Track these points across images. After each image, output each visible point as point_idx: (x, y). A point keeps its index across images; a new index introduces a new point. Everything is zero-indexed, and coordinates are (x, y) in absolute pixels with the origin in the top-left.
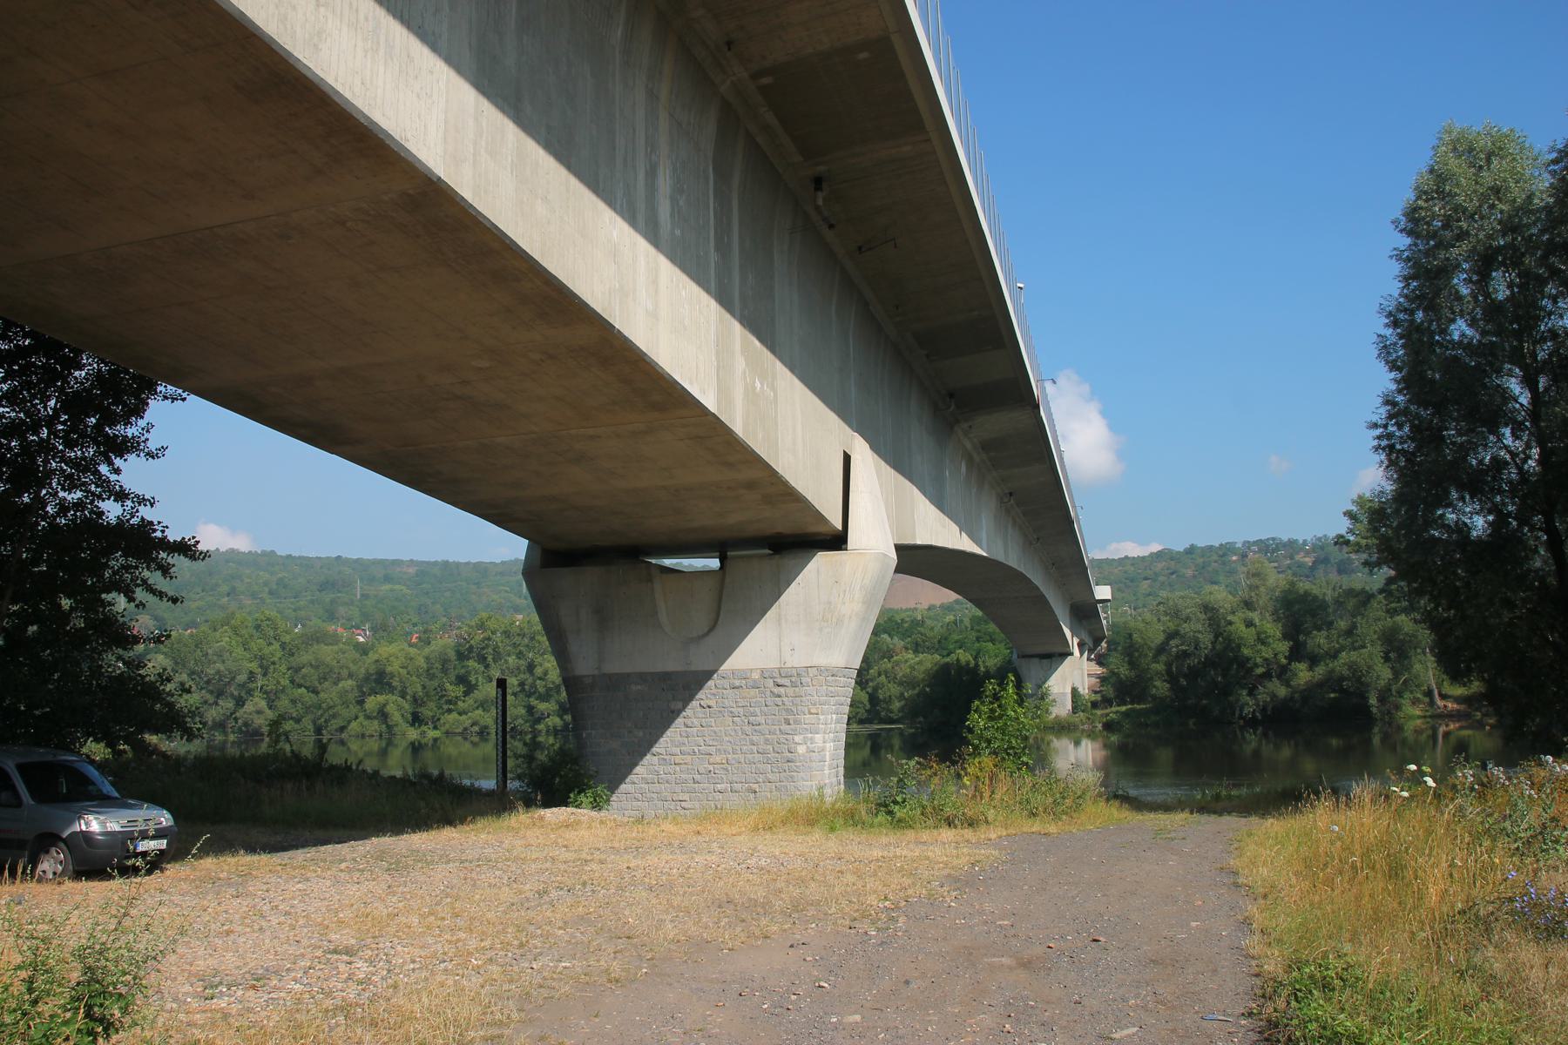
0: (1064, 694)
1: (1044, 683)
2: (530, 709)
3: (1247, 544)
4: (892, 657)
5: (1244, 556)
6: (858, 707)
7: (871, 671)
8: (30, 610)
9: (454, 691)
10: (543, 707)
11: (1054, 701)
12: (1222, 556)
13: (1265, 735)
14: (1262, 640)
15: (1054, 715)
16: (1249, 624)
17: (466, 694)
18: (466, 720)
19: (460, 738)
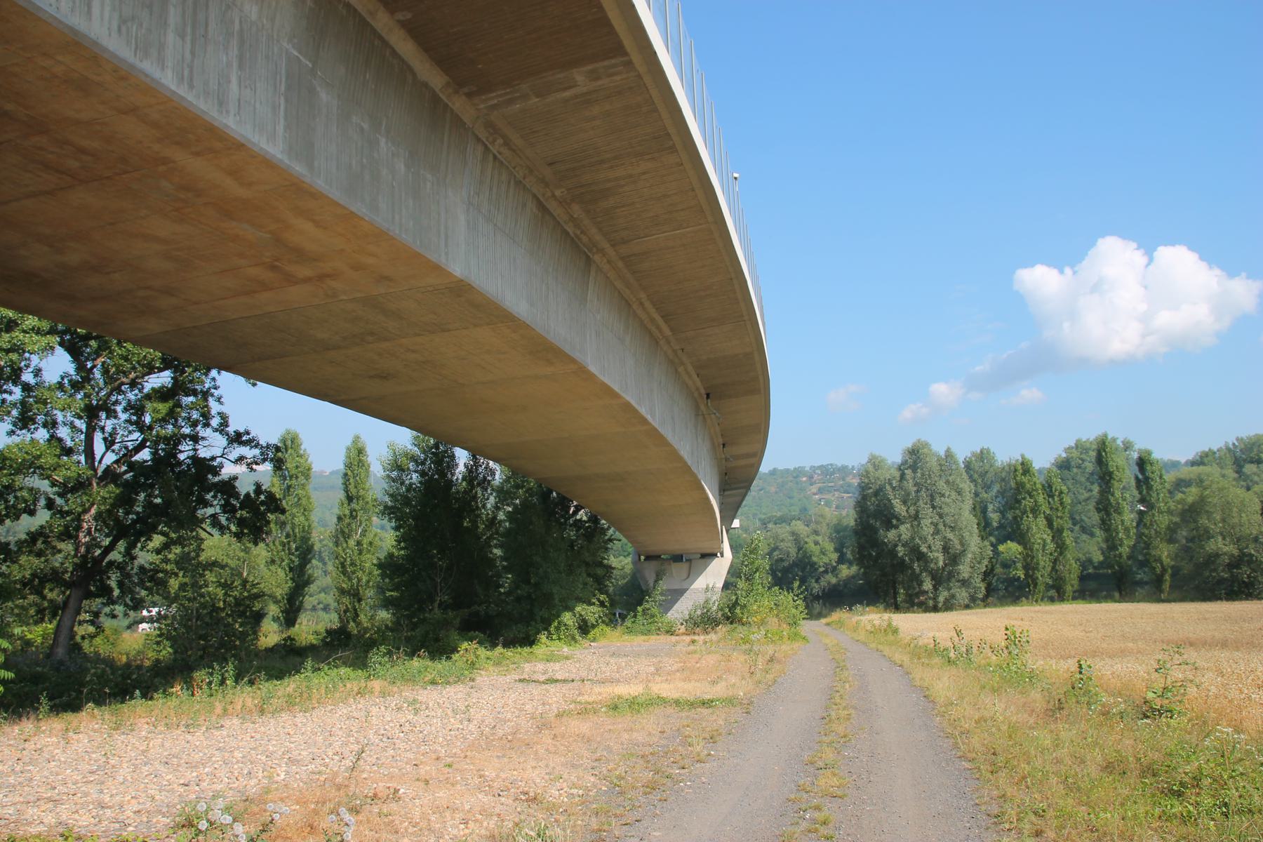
12: (795, 477)
14: (823, 553)
16: (816, 543)
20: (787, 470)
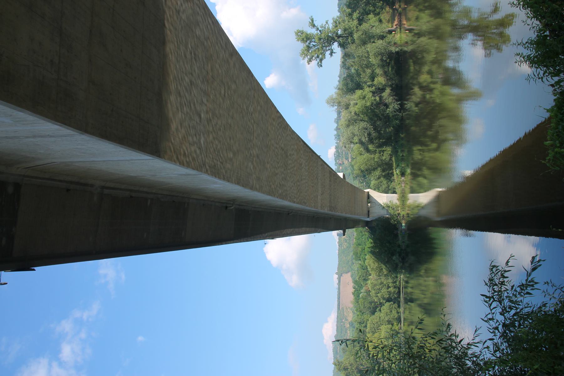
0: (387, 197)
4: (370, 291)
5: (340, 164)
6: (392, 307)
8: (505, 374)
11: (390, 202)
13: (407, 100)
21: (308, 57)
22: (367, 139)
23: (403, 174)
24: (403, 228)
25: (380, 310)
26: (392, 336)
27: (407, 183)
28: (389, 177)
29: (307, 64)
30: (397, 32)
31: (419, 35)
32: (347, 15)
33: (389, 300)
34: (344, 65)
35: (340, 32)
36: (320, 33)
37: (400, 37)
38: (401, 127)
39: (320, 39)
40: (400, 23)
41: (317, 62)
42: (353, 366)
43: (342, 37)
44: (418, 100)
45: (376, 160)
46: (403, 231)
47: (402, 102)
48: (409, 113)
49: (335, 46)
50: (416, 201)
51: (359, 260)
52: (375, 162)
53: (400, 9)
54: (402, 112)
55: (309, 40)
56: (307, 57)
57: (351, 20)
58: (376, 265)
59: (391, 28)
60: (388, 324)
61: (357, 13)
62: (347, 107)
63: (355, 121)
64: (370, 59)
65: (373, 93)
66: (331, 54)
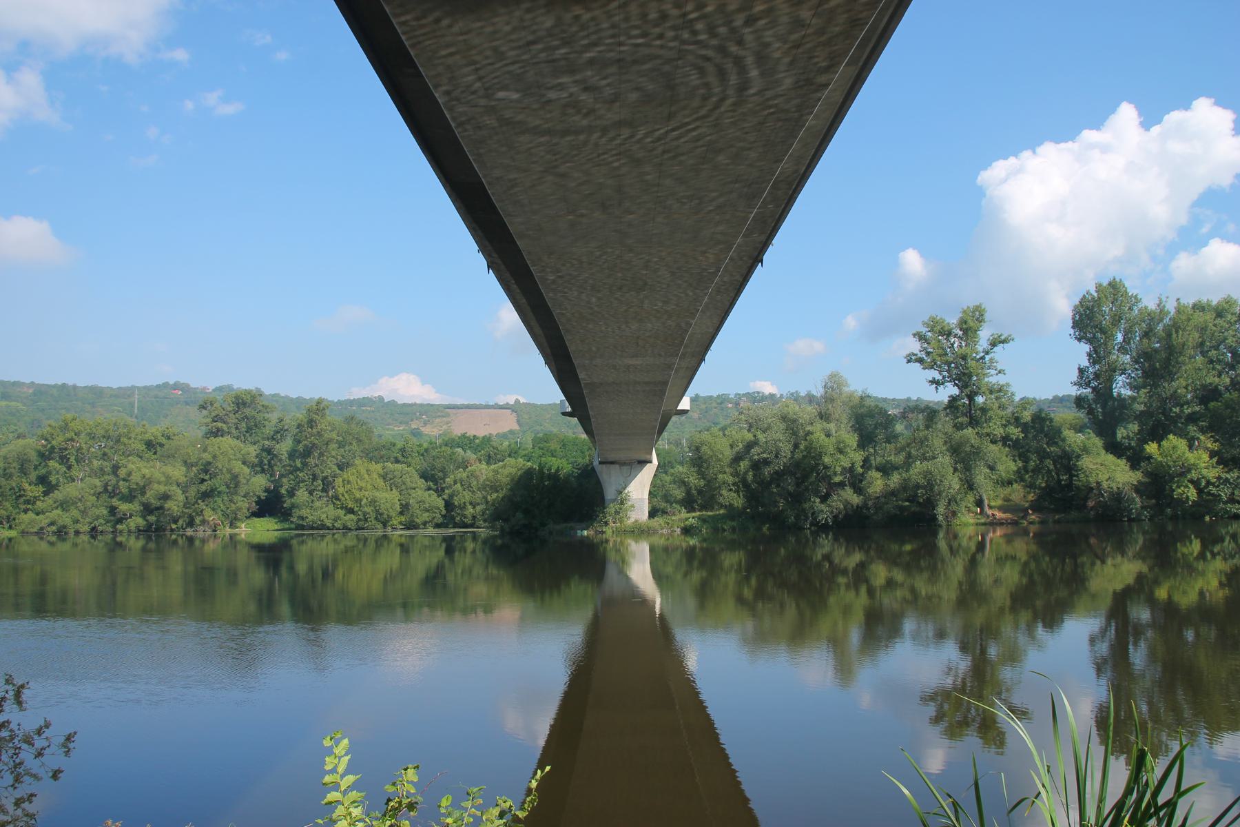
0: (642, 500)
1: (625, 489)
2: (113, 510)
3: (738, 396)
4: (467, 467)
5: (737, 404)
6: (435, 513)
7: (447, 480)
9: (34, 491)
10: (124, 507)
11: (633, 506)
12: (721, 403)
13: (836, 539)
15: (632, 520)
17: (46, 494)
18: (43, 520)
19: (36, 538)
20: (711, 397)
21: (929, 334)
22: (756, 457)
23: (687, 531)
24: (579, 531)
25: (429, 489)
26: (378, 514)
27: (668, 539)
28: (689, 503)
29: (915, 332)
30: (979, 517)
31: (973, 563)
32: (1016, 415)
33: (449, 505)
34: (912, 409)
35: (980, 400)
36: (978, 357)
37: (967, 523)
38: (782, 527)
39: (964, 358)
40: (996, 524)
41: (916, 352)
42: (318, 438)
43: (970, 403)
44: (837, 561)
45: (720, 476)
46: (572, 532)
47: (1138, 520)
48: (811, 543)
49: (951, 390)
50: (634, 557)
51: (533, 445)
52: (716, 475)
53: (1025, 523)
54: (813, 528)
55: (963, 335)
56: (929, 331)
57: (1004, 422)
58: (505, 480)
59: (988, 506)
60: (401, 504)
61: (1018, 436)
62: (824, 416)
63: (795, 434)
64: (919, 462)
65: (851, 469)
66: (934, 382)
